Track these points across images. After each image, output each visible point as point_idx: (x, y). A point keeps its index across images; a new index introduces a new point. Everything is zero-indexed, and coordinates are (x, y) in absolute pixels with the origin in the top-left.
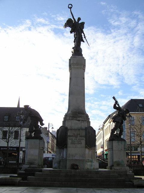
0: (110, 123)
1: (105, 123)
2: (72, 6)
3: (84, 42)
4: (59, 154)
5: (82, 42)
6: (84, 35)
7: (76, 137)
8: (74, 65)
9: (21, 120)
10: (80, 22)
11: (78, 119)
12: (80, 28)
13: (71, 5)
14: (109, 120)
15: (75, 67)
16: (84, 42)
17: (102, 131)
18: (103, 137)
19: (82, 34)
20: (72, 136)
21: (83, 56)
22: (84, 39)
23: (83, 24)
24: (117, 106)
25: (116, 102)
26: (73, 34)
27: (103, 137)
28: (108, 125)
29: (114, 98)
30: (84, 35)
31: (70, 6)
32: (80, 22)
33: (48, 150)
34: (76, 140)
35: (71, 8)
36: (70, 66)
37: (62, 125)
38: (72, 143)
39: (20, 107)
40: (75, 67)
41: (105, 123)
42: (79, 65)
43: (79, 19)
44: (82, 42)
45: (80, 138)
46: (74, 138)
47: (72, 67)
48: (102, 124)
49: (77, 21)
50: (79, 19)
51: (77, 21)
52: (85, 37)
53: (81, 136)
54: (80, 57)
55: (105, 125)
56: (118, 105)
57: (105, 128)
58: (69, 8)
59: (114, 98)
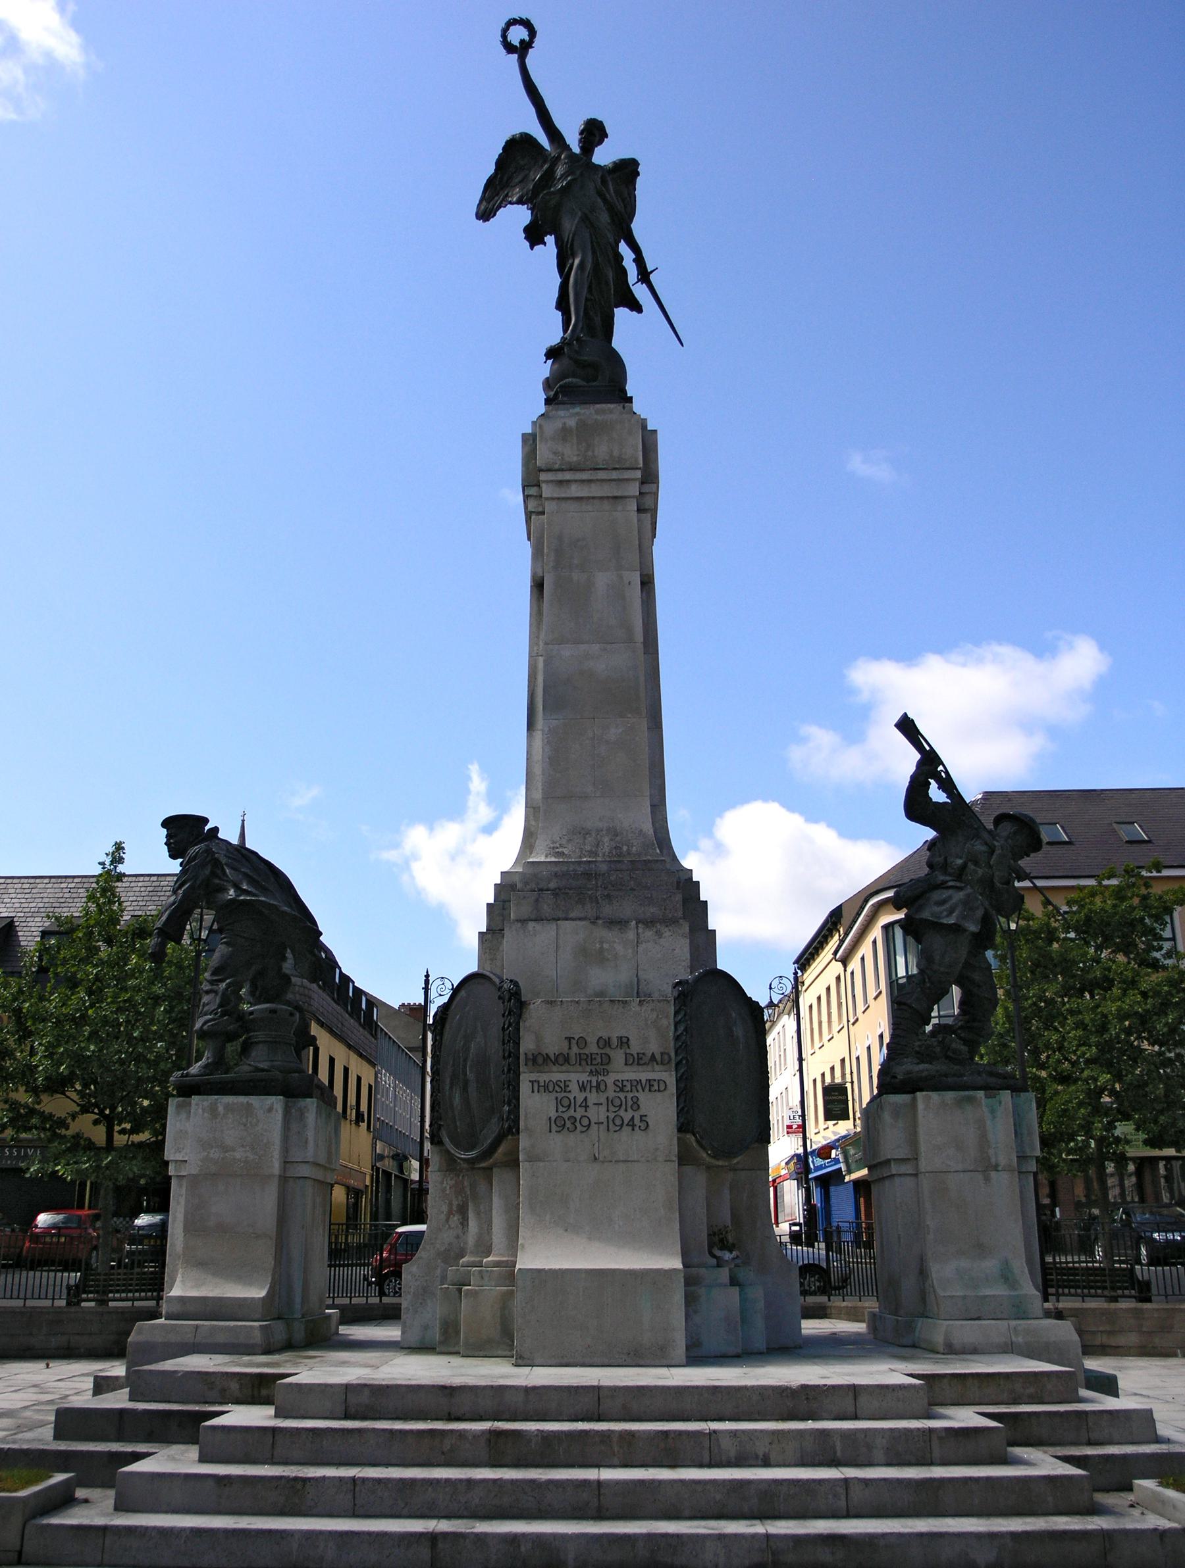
0: (845, 962)
1: (805, 960)
2: (532, 32)
3: (636, 307)
4: (456, 1219)
5: (621, 314)
6: (640, 261)
7: (597, 1063)
8: (560, 476)
9: (190, 970)
10: (603, 156)
11: (607, 910)
12: (605, 200)
13: (527, 24)
14: (834, 942)
15: (575, 491)
16: (636, 307)
17: (793, 1017)
18: (801, 1059)
19: (623, 248)
20: (563, 1060)
21: (637, 407)
22: (640, 292)
23: (627, 170)
24: (936, 794)
25: (930, 763)
26: (549, 249)
27: (801, 1059)
28: (829, 978)
29: (907, 727)
30: (640, 261)
31: (517, 35)
32: (603, 156)
33: (908, 993)
34: (593, 1098)
35: (522, 50)
36: (531, 482)
37: (473, 967)
38: (561, 1125)
39: (1050, 1297)
40: (575, 491)
41: (805, 960)
42: (601, 475)
43: (594, 132)
44: (621, 314)
45: (630, 1074)
46: (576, 1077)
47: (547, 491)
48: (789, 970)
49: (576, 149)
50: (594, 132)
51: (576, 149)
52: (644, 276)
53: (637, 1060)
54: (609, 411)
55: (809, 976)
56: (947, 784)
57: (807, 999)
58: (509, 48)
59: (907, 727)
